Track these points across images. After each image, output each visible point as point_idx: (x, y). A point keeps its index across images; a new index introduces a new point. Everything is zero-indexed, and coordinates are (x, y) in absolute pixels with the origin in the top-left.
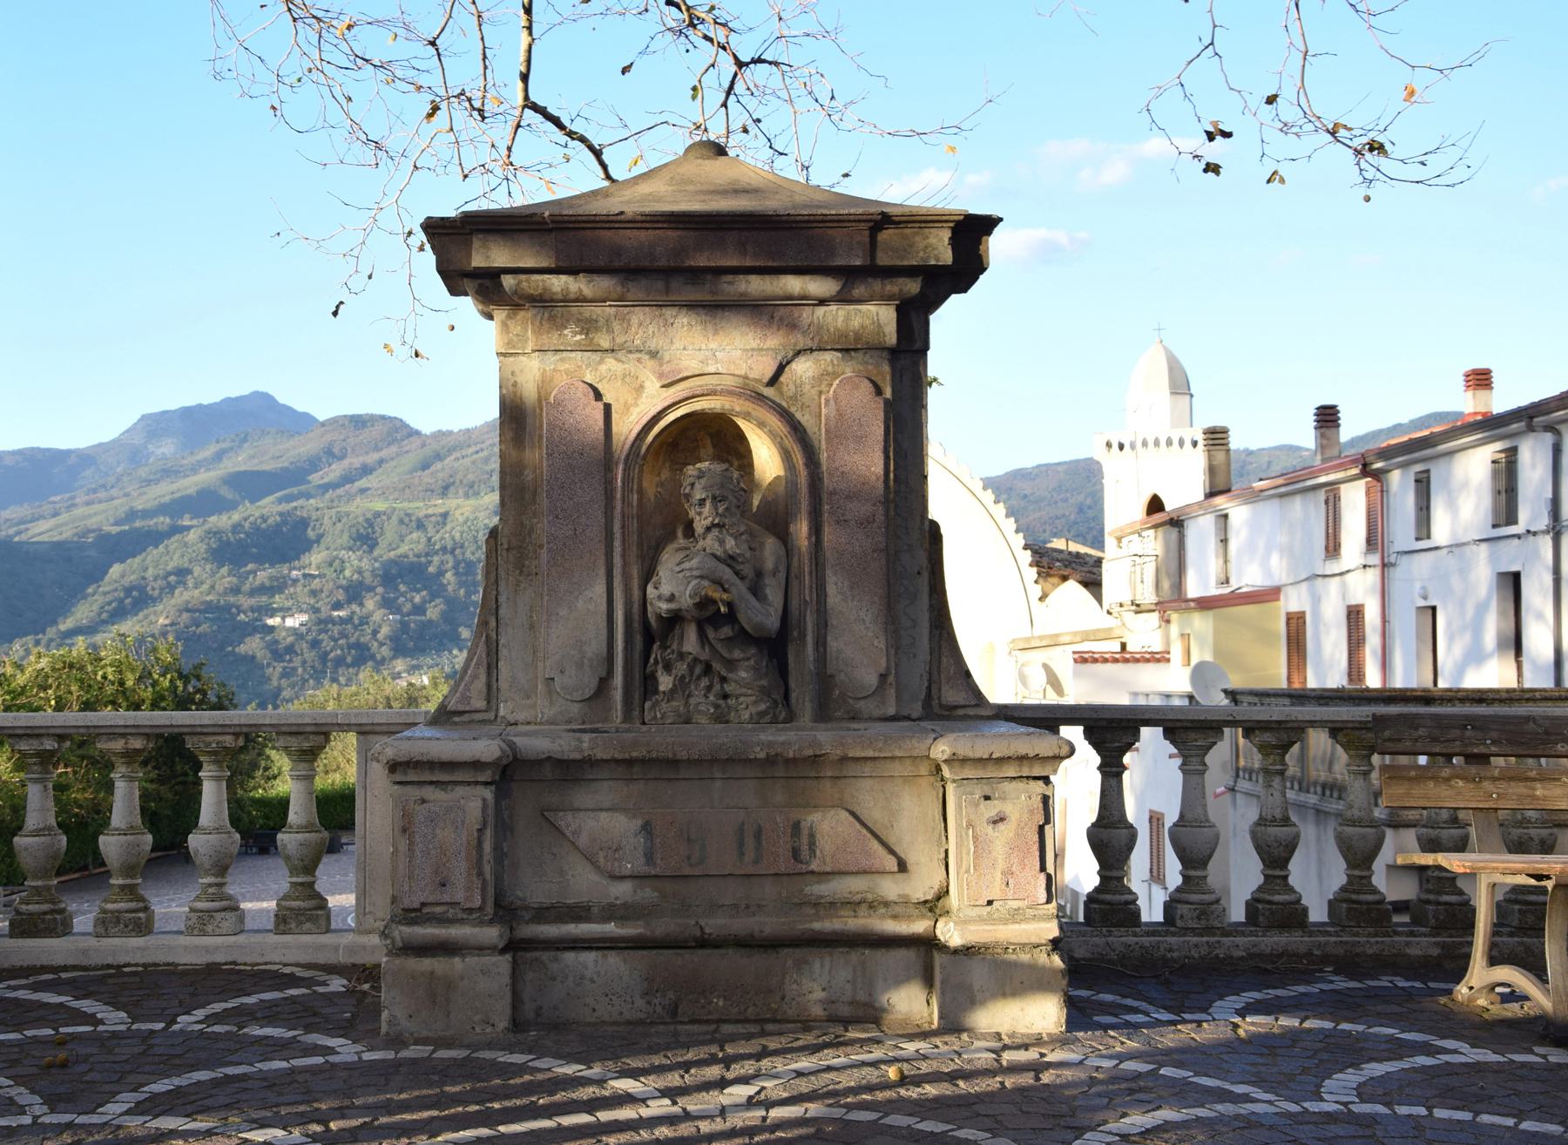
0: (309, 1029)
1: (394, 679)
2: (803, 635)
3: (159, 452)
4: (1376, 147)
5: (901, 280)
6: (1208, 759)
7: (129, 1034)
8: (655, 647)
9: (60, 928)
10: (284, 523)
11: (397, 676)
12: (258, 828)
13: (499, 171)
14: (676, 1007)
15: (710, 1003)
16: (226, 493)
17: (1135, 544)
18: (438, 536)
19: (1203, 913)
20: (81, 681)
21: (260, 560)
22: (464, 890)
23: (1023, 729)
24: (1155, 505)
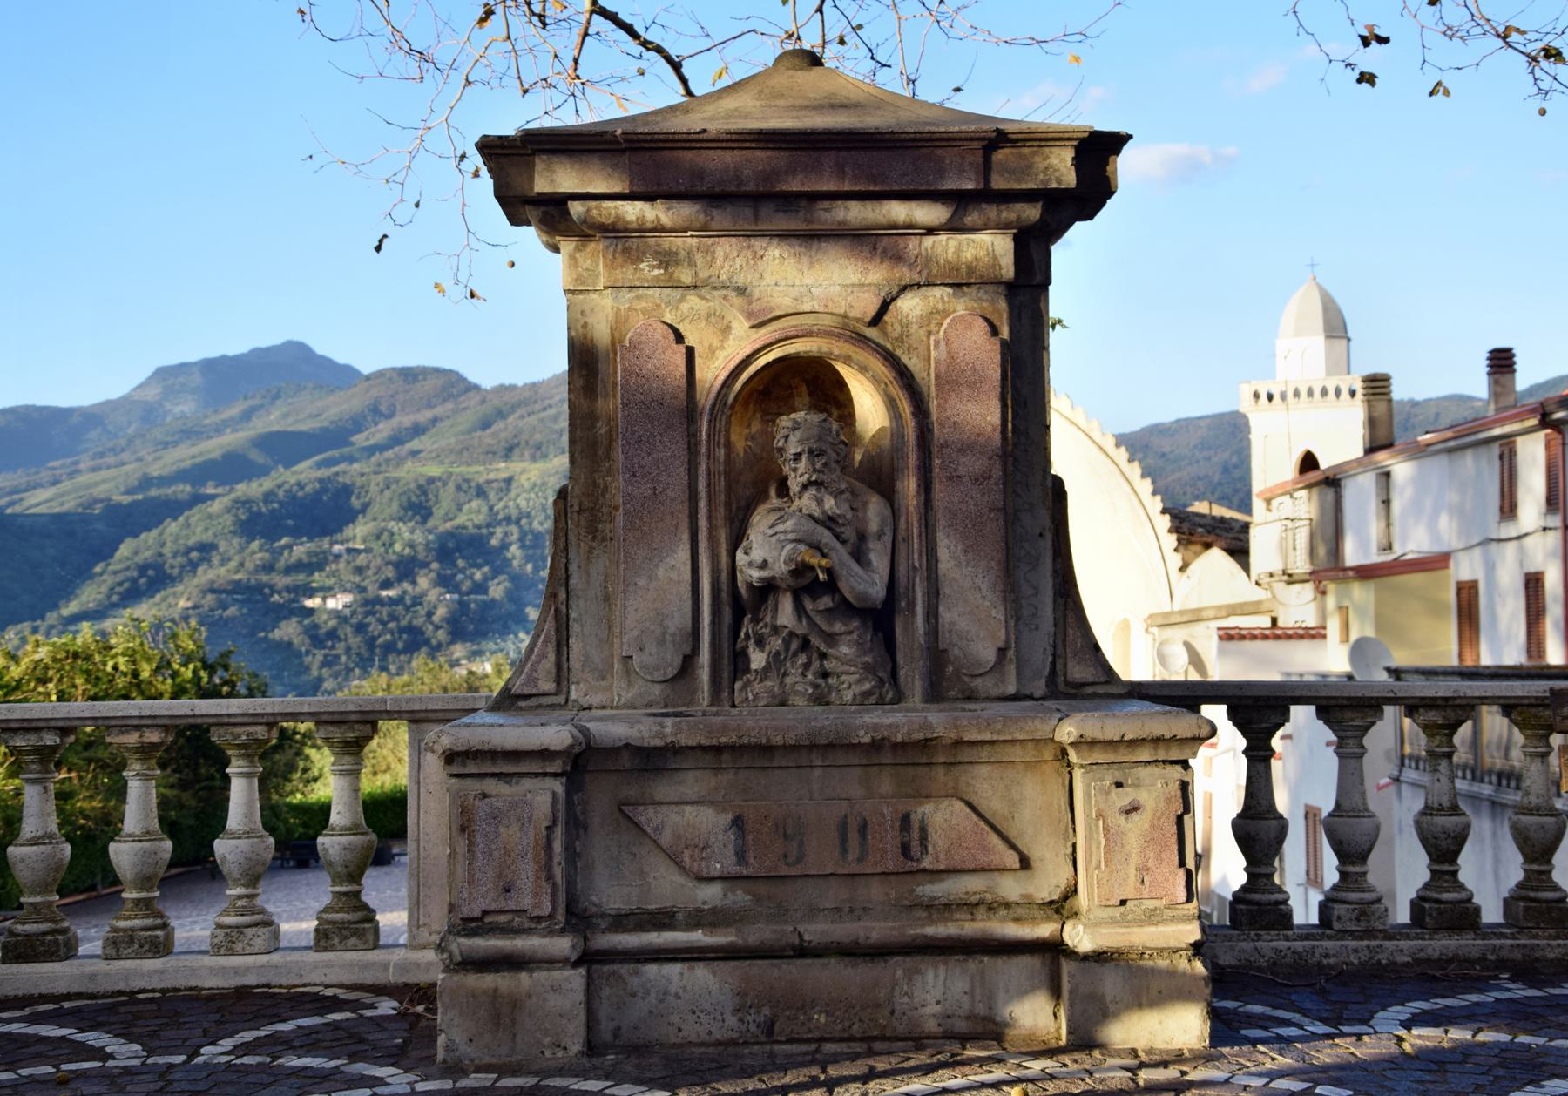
0: (354, 1057)
1: (452, 666)
2: (912, 605)
3: (178, 409)
4: (1551, 54)
5: (1018, 206)
6: (1366, 741)
7: (143, 1070)
8: (746, 620)
9: (62, 951)
10: (324, 490)
11: (455, 663)
12: (295, 840)
13: (563, 87)
14: (773, 1025)
15: (811, 1019)
16: (257, 456)
17: (1284, 506)
18: (501, 504)
19: (1363, 913)
20: (88, 672)
21: (296, 533)
22: (531, 896)
23: (1158, 708)
24: (1309, 462)
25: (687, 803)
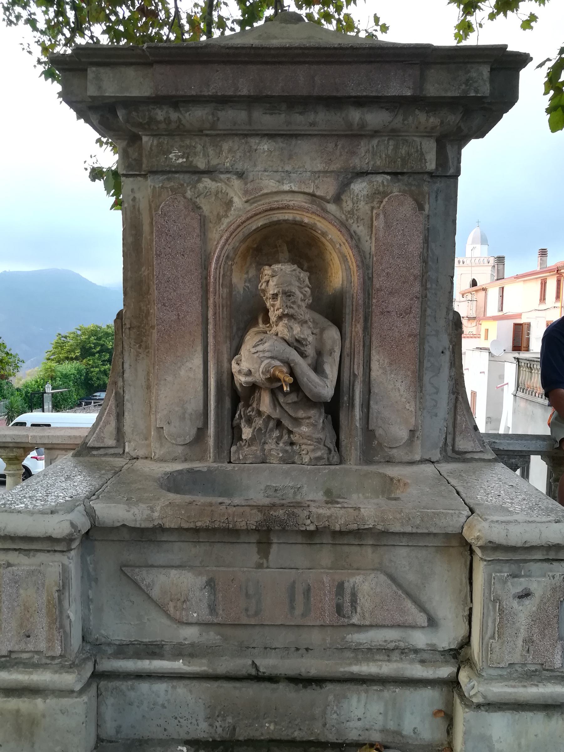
8: (241, 404)
15: (262, 726)
25: (172, 567)
